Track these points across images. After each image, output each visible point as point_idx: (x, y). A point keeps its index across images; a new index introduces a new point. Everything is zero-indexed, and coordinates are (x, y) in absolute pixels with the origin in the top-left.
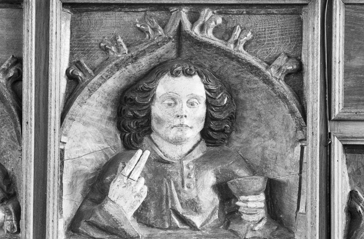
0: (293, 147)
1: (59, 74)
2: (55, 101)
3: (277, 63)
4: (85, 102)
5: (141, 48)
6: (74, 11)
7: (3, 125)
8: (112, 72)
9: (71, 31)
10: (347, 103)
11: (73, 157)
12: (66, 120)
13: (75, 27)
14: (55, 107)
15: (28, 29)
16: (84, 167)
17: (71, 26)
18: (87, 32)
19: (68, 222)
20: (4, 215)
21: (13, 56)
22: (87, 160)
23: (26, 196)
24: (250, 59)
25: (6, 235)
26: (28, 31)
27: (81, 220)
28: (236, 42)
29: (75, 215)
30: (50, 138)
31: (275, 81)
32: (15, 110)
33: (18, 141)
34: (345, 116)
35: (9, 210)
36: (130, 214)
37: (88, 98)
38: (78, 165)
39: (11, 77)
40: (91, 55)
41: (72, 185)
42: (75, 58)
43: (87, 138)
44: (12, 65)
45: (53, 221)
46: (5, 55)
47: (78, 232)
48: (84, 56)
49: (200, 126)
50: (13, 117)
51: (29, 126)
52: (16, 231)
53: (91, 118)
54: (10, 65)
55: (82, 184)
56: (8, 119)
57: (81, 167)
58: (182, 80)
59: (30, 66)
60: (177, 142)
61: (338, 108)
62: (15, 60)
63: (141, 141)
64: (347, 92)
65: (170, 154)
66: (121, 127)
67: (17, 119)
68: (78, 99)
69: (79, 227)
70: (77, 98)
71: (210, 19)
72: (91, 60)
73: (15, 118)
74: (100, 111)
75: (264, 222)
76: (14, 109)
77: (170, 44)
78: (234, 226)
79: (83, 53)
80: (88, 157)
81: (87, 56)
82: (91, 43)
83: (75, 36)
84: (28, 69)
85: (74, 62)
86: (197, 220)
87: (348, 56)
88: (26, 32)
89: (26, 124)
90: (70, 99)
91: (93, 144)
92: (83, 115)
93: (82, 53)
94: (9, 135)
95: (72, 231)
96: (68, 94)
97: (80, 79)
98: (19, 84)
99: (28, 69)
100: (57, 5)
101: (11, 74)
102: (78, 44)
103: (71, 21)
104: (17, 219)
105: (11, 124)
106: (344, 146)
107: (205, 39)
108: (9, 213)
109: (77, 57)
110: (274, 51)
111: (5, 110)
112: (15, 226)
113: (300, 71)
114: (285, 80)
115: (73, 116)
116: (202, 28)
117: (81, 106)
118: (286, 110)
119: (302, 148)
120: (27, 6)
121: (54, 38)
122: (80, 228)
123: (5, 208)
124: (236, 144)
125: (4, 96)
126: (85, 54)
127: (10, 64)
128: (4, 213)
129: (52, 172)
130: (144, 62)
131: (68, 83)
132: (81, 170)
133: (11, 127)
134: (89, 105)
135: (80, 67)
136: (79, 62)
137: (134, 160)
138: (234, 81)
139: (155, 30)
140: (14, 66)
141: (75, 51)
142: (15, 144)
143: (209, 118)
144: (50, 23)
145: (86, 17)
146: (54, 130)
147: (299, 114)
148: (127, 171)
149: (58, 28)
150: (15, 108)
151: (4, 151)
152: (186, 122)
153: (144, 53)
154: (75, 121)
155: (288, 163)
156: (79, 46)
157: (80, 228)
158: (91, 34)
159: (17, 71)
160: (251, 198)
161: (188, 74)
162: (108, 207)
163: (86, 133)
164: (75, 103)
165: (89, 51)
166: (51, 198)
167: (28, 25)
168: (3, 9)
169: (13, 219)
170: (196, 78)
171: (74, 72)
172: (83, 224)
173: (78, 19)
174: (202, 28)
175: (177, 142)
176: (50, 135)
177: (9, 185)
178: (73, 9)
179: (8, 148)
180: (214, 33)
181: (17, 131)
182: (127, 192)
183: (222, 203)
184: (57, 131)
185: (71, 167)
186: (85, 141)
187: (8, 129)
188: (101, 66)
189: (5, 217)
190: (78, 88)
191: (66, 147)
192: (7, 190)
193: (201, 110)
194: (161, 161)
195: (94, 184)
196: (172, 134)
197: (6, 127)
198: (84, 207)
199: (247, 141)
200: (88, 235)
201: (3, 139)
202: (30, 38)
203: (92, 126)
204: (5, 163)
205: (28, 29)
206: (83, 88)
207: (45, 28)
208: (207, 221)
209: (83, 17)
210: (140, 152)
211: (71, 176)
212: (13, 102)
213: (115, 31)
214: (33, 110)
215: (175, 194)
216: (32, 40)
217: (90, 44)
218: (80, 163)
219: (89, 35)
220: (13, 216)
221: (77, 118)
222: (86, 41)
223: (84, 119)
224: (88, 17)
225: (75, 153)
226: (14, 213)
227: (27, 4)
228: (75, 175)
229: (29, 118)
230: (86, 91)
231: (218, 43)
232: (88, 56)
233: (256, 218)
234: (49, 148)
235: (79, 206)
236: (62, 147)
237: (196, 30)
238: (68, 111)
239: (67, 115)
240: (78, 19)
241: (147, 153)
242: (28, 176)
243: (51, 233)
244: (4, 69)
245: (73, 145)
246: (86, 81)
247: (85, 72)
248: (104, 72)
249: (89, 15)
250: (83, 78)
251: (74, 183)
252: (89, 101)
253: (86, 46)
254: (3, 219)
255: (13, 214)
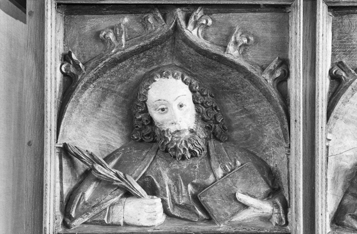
1: (325, 75)
2: (322, 100)
4: (348, 101)
6: (336, 14)
7: (267, 123)
9: (333, 33)
11: (335, 154)
12: (331, 118)
13: (336, 29)
14: (322, 106)
15: (295, 32)
16: (344, 163)
17: (332, 28)
18: (348, 34)
19: (332, 216)
20: (272, 208)
21: (279, 57)
22: (347, 156)
23: (295, 190)
25: (275, 227)
26: (296, 34)
27: (345, 213)
29: (338, 209)
30: (318, 135)
32: (283, 109)
33: (284, 138)
35: (276, 203)
37: (351, 97)
38: (339, 161)
39: (277, 78)
40: (352, 55)
41: (334, 180)
42: (337, 59)
43: (347, 135)
44: (279, 66)
45: (322, 214)
46: (269, 57)
47: (343, 225)
48: (345, 57)
50: (280, 116)
51: (298, 124)
52: (284, 223)
53: (352, 116)
54: (276, 66)
55: (343, 179)
56: (274, 118)
57: (342, 163)
59: (298, 67)
62: (280, 61)
67: (285, 117)
68: (342, 99)
69: (343, 220)
70: (342, 97)
72: (352, 61)
73: (282, 117)
76: (281, 108)
79: (344, 54)
80: (348, 153)
81: (348, 57)
82: (352, 44)
83: (336, 37)
84: (296, 70)
85: (336, 62)
88: (293, 35)
89: (295, 122)
90: (334, 98)
91: (352, 141)
92: (346, 113)
93: (344, 54)
94: (273, 132)
95: (337, 224)
96: (330, 94)
97: (343, 79)
98: (284, 83)
99: (296, 70)
100: (323, 9)
101: (277, 75)
102: (340, 45)
103: (332, 24)
104: (285, 212)
105: (277, 122)
108: (277, 207)
109: (339, 58)
111: (271, 110)
112: (284, 219)
115: (337, 114)
117: (344, 105)
120: (294, 10)
121: (321, 40)
122: (344, 221)
123: (273, 202)
125: (272, 96)
126: (346, 55)
127: (277, 65)
128: (273, 207)
129: (320, 168)
131: (331, 83)
132: (341, 166)
133: (277, 125)
134: (351, 104)
135: (343, 68)
136: (341, 62)
140: (280, 67)
141: (337, 52)
142: (280, 141)
144: (317, 26)
145: (347, 20)
146: (322, 128)
149: (325, 31)
150: (282, 107)
151: (267, 148)
154: (338, 119)
156: (340, 48)
157: (344, 221)
158: (352, 35)
159: (283, 72)
163: (346, 130)
164: (340, 102)
165: (350, 52)
166: (320, 193)
167: (296, 29)
168: (268, 13)
169: (281, 212)
171: (337, 73)
172: (348, 218)
173: (339, 21)
176: (318, 132)
177: (273, 180)
178: (335, 12)
179: (271, 145)
181: (284, 130)
184: (324, 128)
185: (333, 163)
186: (346, 138)
187: (273, 127)
189: (273, 210)
190: (341, 87)
191: (330, 144)
192: (272, 185)
195: (353, 179)
197: (270, 125)
198: (346, 201)
200: (354, 228)
201: (267, 136)
202: (298, 40)
203: (352, 124)
204: (267, 159)
205: (295, 32)
206: (346, 88)
207: (311, 31)
209: (344, 20)
211: (334, 172)
212: (280, 101)
214: (302, 109)
216: (300, 42)
217: (351, 45)
218: (341, 159)
219: (351, 36)
220: (281, 210)
221: (340, 117)
222: (348, 42)
223: (346, 117)
224: (349, 20)
225: (337, 150)
226: (282, 207)
227: (294, 8)
228: (337, 170)
229: (298, 117)
232: (349, 57)
234: (316, 145)
235: (340, 200)
238: (333, 110)
239: (332, 114)
240: (339, 21)
242: (297, 171)
243: (320, 226)
244: (271, 70)
245: (336, 142)
246: (349, 81)
247: (348, 72)
249: (350, 17)
250: (346, 77)
251: (336, 178)
252: (351, 100)
253: (347, 47)
254: (272, 212)
255: (281, 207)
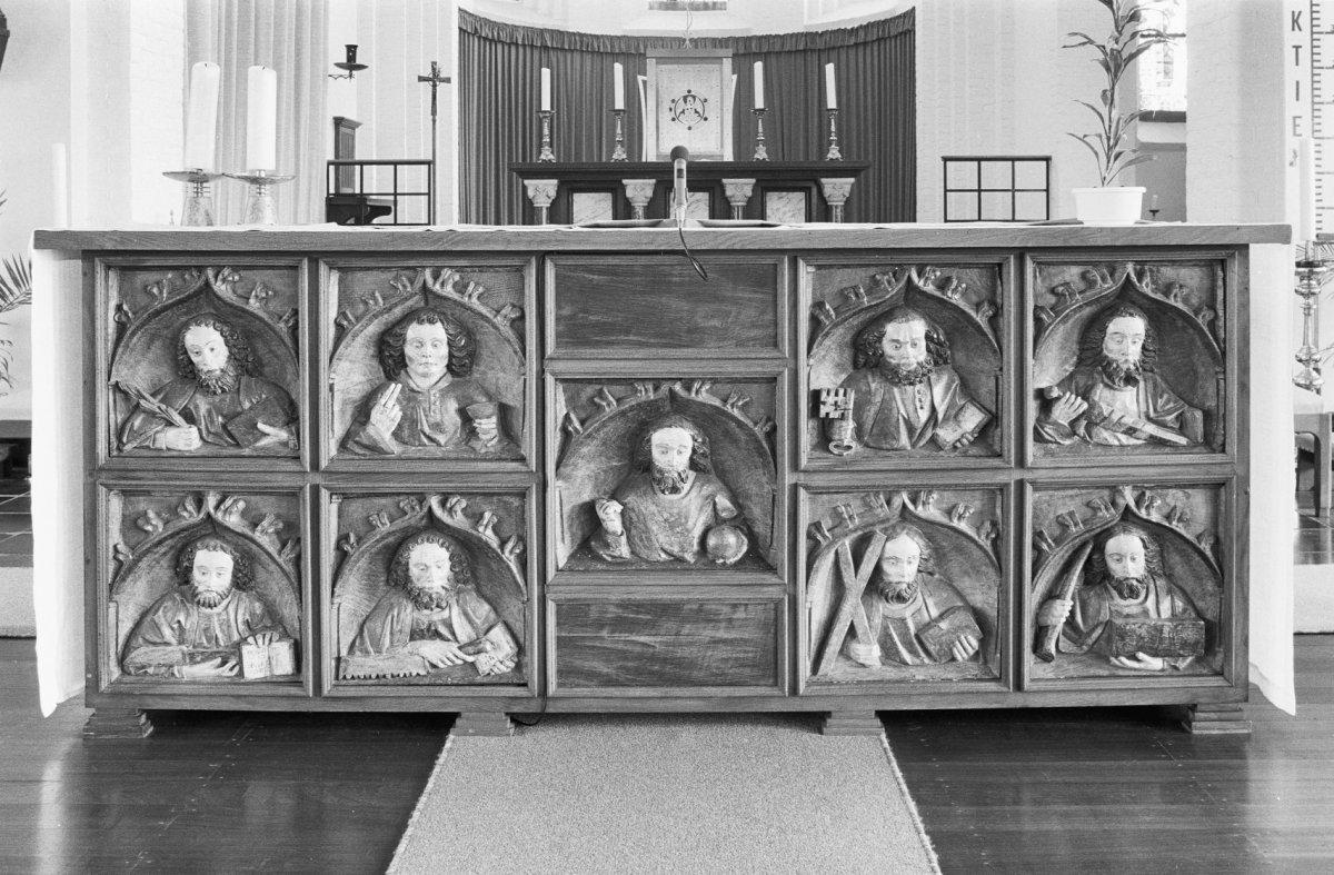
0: (519, 379)
3: (503, 312)
5: (393, 301)
8: (371, 320)
10: (558, 345)
12: (334, 360)
24: (484, 310)
28: (470, 295)
31: (501, 328)
34: (335, 693)
36: (387, 436)
41: (343, 412)
49: (446, 362)
58: (427, 326)
60: (425, 375)
61: (550, 349)
63: (399, 373)
64: (558, 335)
65: (421, 385)
66: (382, 362)
68: (344, 344)
71: (449, 278)
74: (365, 350)
75: (496, 440)
77: (417, 297)
78: (474, 443)
86: (442, 439)
87: (558, 306)
106: (556, 380)
107: (444, 294)
108: (292, 434)
110: (501, 302)
113: (522, 317)
114: (511, 326)
116: (443, 284)
118: (511, 350)
119: (525, 380)
124: (476, 375)
130: (398, 312)
137: (388, 392)
138: (470, 325)
139: (404, 286)
143: (451, 356)
147: (520, 354)
148: (383, 401)
152: (430, 360)
153: (396, 305)
155: (515, 392)
160: (483, 421)
161: (431, 322)
162: (370, 430)
170: (439, 324)
174: (443, 284)
175: (425, 375)
180: (454, 287)
182: (383, 417)
183: (463, 424)
186: (352, 375)
188: (364, 315)
193: (444, 350)
194: (413, 390)
196: (421, 369)
199: (484, 373)
208: (450, 439)
210: (393, 385)
213: (373, 287)
215: (423, 418)
228: (345, 402)
230: (349, 336)
231: (456, 296)
233: (488, 437)
236: (331, 382)
237: (437, 287)
241: (400, 386)
247: (349, 321)
248: (364, 322)
